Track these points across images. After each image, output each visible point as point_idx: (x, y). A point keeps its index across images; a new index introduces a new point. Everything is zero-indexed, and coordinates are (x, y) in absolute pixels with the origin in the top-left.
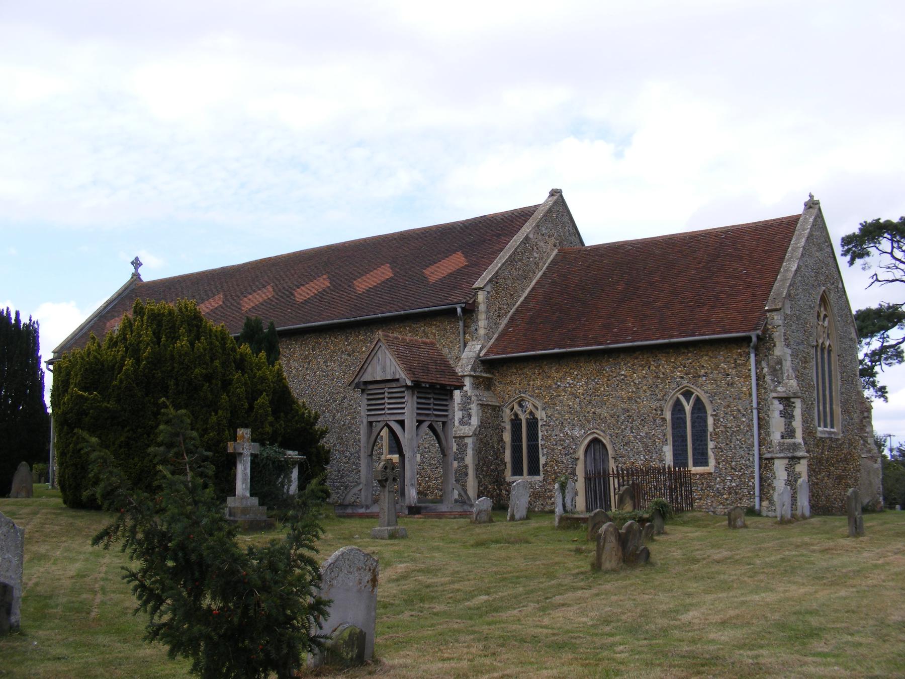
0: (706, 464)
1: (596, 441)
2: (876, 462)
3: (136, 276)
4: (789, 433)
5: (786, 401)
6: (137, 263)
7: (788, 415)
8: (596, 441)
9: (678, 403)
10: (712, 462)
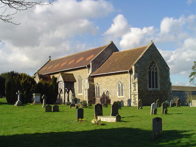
0: (123, 95)
1: (108, 91)
2: (172, 95)
3: (50, 60)
4: (135, 90)
5: (134, 83)
6: (50, 57)
7: (135, 87)
8: (108, 91)
9: (119, 84)
10: (124, 95)
